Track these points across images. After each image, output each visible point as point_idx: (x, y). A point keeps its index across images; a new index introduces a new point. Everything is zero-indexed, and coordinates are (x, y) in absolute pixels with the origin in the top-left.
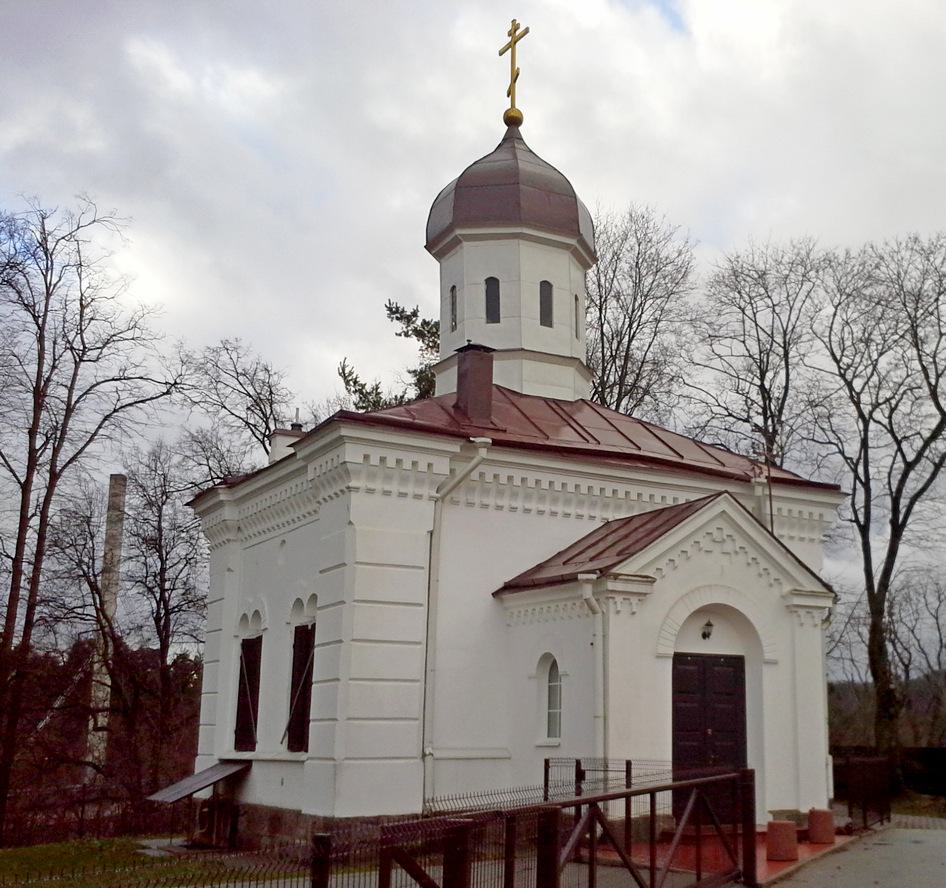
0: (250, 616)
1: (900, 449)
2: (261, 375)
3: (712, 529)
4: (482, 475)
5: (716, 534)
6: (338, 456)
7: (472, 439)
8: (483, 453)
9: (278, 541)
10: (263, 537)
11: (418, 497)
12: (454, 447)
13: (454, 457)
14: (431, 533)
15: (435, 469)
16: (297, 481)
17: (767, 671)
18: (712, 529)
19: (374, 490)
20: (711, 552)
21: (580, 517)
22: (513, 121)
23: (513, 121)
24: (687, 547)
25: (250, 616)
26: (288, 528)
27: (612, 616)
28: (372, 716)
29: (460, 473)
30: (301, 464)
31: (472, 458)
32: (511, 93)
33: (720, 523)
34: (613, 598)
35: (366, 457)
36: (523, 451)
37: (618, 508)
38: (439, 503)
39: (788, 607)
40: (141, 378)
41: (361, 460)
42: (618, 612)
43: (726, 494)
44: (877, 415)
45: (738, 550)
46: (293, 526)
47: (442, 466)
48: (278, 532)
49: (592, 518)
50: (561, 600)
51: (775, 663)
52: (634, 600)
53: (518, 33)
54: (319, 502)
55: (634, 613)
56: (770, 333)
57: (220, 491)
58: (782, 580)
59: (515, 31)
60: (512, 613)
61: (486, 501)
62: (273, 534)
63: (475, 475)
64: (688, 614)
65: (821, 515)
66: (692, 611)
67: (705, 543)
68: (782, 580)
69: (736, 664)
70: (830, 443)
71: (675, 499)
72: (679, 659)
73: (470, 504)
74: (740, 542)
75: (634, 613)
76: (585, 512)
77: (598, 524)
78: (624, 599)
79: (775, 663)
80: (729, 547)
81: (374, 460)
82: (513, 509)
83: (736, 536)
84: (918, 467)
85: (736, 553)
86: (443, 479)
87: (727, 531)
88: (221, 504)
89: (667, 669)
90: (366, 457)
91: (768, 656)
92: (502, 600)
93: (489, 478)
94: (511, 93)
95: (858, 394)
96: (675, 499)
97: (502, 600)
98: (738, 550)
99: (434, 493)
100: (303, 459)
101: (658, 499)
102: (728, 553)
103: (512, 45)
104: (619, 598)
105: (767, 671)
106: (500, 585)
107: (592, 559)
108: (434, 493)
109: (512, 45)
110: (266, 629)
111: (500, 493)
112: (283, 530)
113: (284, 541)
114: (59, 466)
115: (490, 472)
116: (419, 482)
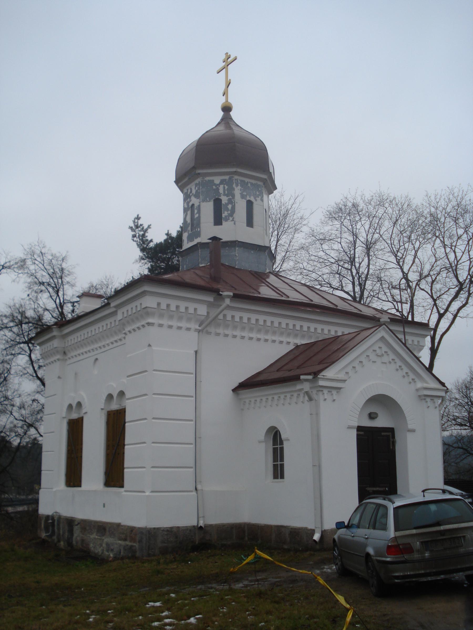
0: (74, 405)
1: (435, 304)
2: (19, 269)
3: (376, 348)
4: (225, 316)
5: (379, 352)
6: (141, 304)
7: (221, 293)
8: (228, 301)
9: (94, 358)
10: (82, 357)
11: (189, 329)
12: (210, 298)
13: (210, 305)
14: (196, 352)
15: (199, 312)
16: (112, 320)
17: (409, 435)
18: (376, 348)
19: (163, 325)
20: (375, 362)
21: (281, 342)
22: (227, 109)
23: (227, 109)
24: (363, 358)
25: (74, 405)
26: (100, 351)
27: (322, 403)
28: (157, 465)
29: (212, 315)
30: (113, 310)
31: (221, 305)
32: (225, 93)
33: (381, 344)
34: (322, 391)
35: (159, 304)
36: (73, 324)
37: (303, 337)
38: (201, 333)
39: (420, 396)
40: (295, 200)
41: (156, 306)
42: (325, 400)
43: (384, 326)
44: (423, 284)
45: (391, 361)
46: (103, 349)
47: (202, 310)
48: (92, 354)
49: (288, 343)
50: (275, 394)
51: (413, 431)
52: (334, 392)
53: (229, 60)
54: (125, 334)
55: (334, 400)
56: (357, 239)
57: (54, 330)
58: (416, 380)
59: (228, 59)
60: (245, 402)
61: (227, 332)
62: (89, 354)
63: (221, 317)
64: (364, 401)
65: (418, 342)
66: (367, 398)
67: (373, 357)
68: (416, 380)
69: (391, 431)
70: (388, 301)
71: (336, 332)
72: (359, 429)
73: (218, 334)
74: (392, 356)
75: (334, 400)
76: (284, 339)
77: (292, 347)
78: (329, 391)
79: (413, 431)
80: (385, 359)
81: (164, 306)
82: (235, 337)
83: (390, 352)
84: (445, 317)
85: (390, 362)
86: (203, 318)
87: (385, 349)
88: (53, 338)
89: (354, 433)
90: (159, 304)
91: (410, 427)
92: (238, 394)
93: (229, 318)
94: (225, 93)
95: (407, 274)
96: (343, 332)
97: (238, 394)
98: (391, 361)
99: (197, 327)
100: (115, 307)
101: (326, 332)
102: (385, 363)
103: (225, 68)
104: (325, 391)
105: (409, 435)
106: (236, 385)
107: (298, 367)
108: (197, 327)
109: (225, 68)
110: (86, 413)
111: (235, 328)
112: (96, 352)
113: (97, 359)
114: (58, 297)
115: (229, 314)
116: (189, 320)
